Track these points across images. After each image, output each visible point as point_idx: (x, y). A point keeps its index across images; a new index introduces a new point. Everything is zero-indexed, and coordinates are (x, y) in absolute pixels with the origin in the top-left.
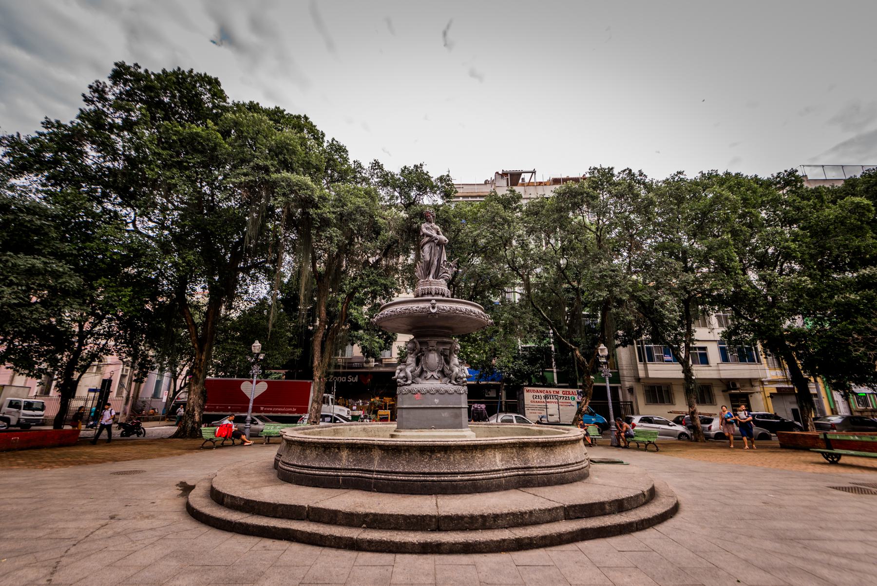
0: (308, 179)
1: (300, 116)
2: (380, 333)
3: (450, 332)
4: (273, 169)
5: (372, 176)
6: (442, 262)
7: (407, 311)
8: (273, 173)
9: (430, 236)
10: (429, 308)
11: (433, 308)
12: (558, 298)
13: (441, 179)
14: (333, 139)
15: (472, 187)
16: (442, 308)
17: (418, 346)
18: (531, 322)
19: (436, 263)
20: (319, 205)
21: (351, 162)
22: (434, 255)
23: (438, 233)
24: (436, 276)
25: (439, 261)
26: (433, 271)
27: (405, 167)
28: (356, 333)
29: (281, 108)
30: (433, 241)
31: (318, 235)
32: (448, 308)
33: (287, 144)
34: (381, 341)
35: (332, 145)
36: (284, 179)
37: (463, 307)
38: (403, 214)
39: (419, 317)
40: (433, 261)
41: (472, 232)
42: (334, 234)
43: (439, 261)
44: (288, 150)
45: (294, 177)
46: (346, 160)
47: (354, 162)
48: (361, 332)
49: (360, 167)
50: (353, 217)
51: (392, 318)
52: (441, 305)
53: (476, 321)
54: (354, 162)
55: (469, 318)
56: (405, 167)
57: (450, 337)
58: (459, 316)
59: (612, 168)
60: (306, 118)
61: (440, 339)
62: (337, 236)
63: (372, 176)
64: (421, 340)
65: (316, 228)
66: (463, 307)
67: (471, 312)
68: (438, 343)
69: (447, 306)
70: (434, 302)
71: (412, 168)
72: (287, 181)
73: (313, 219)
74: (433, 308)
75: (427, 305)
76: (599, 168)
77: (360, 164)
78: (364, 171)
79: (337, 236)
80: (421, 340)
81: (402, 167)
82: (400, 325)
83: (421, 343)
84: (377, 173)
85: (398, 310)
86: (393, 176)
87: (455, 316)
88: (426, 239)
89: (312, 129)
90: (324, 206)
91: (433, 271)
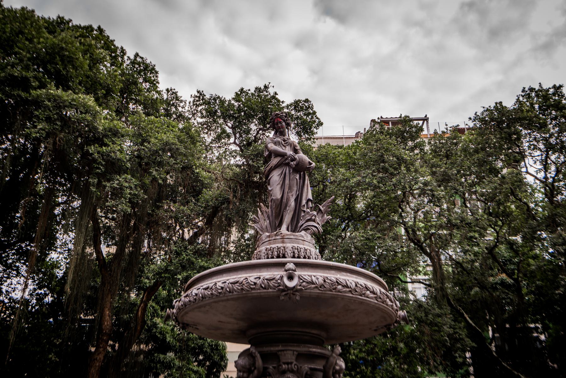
0: (90, 101)
1: (90, 27)
2: (201, 357)
3: (323, 334)
4: (35, 84)
5: (194, 115)
6: (304, 202)
7: (236, 287)
8: (35, 89)
9: (282, 155)
10: (282, 277)
11: (291, 278)
12: (486, 294)
13: (296, 105)
14: (137, 55)
15: (341, 140)
16: (309, 279)
17: (259, 362)
18: (451, 331)
19: (292, 203)
20: (106, 140)
21: (162, 87)
22: (290, 188)
23: (296, 151)
24: (294, 227)
25: (298, 200)
26: (287, 219)
27: (242, 90)
28: (162, 356)
29: (67, 18)
30: (288, 164)
31: (99, 185)
32: (321, 280)
33: (62, 48)
34: (201, 369)
35: (133, 63)
36: (50, 98)
37: (351, 280)
38: (239, 160)
39: (260, 298)
40: (288, 200)
41: (347, 180)
42: (127, 185)
43: (298, 200)
44: (63, 58)
45: (67, 96)
46: (154, 84)
47: (167, 90)
48: (171, 355)
49: (177, 98)
50: (159, 159)
51: (206, 301)
52: (306, 274)
53: (377, 309)
54: (167, 90)
55: (362, 302)
56: (242, 90)
57: (320, 343)
58: (343, 298)
59: (561, 86)
60: (100, 30)
61: (303, 349)
62: (131, 188)
63: (194, 115)
64: (266, 349)
65: (98, 175)
66: (351, 280)
67: (367, 288)
68: (301, 356)
69: (318, 276)
70: (291, 266)
71: (252, 91)
72: (55, 100)
73: (94, 160)
74: (291, 278)
75: (277, 273)
76: (537, 88)
77: (176, 93)
78: (182, 104)
79: (131, 188)
80: (266, 349)
81: (237, 90)
82: (223, 318)
83: (265, 357)
84: (201, 112)
85: (220, 284)
86: (222, 102)
87: (334, 298)
88: (275, 161)
89: (109, 45)
90: (114, 143)
91: (287, 219)
